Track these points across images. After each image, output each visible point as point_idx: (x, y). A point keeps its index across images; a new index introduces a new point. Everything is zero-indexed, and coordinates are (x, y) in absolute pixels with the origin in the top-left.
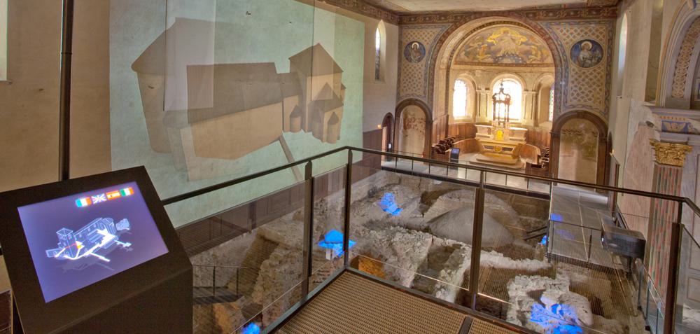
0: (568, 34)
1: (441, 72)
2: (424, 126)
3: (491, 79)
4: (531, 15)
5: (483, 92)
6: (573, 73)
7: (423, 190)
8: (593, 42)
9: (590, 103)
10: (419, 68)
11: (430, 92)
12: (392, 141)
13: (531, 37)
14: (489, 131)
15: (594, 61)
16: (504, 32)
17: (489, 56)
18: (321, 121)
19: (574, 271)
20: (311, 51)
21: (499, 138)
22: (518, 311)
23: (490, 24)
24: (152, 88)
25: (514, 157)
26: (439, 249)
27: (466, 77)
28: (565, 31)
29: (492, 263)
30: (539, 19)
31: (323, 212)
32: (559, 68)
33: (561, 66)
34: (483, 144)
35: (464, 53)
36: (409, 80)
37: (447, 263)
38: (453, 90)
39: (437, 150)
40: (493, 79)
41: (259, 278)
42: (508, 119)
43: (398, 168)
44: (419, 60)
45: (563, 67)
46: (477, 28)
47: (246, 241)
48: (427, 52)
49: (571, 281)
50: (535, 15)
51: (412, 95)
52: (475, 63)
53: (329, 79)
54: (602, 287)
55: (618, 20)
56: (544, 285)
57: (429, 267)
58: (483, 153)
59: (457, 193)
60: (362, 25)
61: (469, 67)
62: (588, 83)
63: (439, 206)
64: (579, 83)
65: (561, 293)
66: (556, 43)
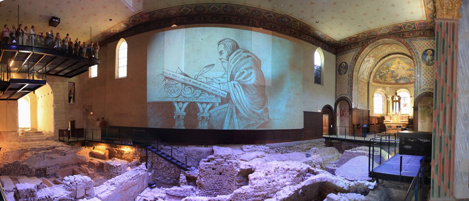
0: (420, 46)
4: (401, 36)
6: (423, 69)
11: (351, 90)
17: (393, 79)
27: (381, 91)
28: (418, 44)
30: (405, 38)
32: (416, 67)
33: (417, 65)
35: (378, 76)
44: (345, 73)
45: (418, 66)
48: (349, 67)
51: (342, 94)
52: (386, 83)
61: (382, 85)
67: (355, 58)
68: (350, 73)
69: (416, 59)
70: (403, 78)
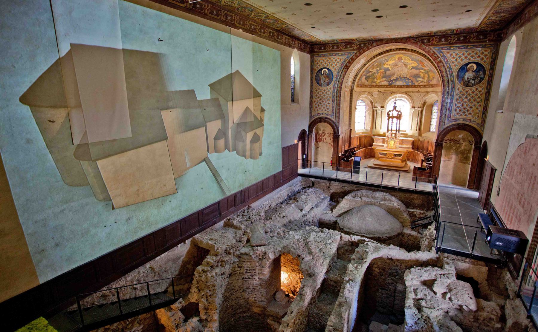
1: (346, 94)
2: (332, 139)
3: (386, 98)
4: (425, 41)
5: (379, 110)
6: (458, 92)
7: (332, 191)
8: (477, 64)
9: (469, 117)
10: (328, 91)
12: (306, 152)
13: (421, 62)
14: (384, 141)
15: (476, 80)
16: (399, 59)
17: (385, 79)
18: (244, 141)
19: (458, 260)
20: (231, 77)
21: (392, 146)
22: (414, 299)
23: (388, 51)
24: (53, 122)
25: (403, 161)
26: (346, 244)
27: (366, 97)
28: (454, 55)
29: (390, 255)
30: (432, 45)
31: (249, 218)
32: (447, 88)
33: (449, 86)
34: (378, 152)
35: (364, 77)
36: (320, 101)
37: (353, 257)
38: (355, 108)
39: (343, 159)
40: (387, 98)
41: (194, 282)
42: (399, 131)
43: (311, 174)
44: (328, 84)
45: (450, 87)
46: (377, 56)
47: (182, 250)
48: (335, 76)
49: (455, 269)
50: (429, 41)
53: (250, 103)
54: (480, 272)
55: (503, 44)
56: (435, 275)
57: (338, 258)
58: (378, 159)
59: (359, 193)
60: (278, 53)
61: (368, 89)
62: (469, 100)
63: (345, 204)
64: (462, 100)
65: (449, 281)
66: (445, 65)
67: (346, 66)
68: (337, 86)
69: (448, 77)
70: (401, 78)
